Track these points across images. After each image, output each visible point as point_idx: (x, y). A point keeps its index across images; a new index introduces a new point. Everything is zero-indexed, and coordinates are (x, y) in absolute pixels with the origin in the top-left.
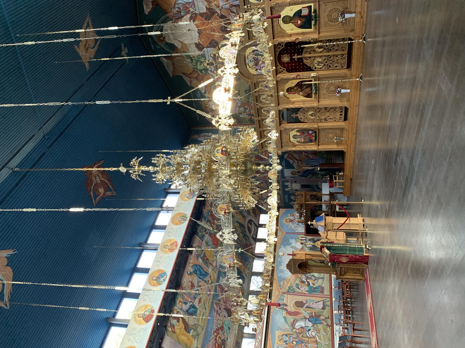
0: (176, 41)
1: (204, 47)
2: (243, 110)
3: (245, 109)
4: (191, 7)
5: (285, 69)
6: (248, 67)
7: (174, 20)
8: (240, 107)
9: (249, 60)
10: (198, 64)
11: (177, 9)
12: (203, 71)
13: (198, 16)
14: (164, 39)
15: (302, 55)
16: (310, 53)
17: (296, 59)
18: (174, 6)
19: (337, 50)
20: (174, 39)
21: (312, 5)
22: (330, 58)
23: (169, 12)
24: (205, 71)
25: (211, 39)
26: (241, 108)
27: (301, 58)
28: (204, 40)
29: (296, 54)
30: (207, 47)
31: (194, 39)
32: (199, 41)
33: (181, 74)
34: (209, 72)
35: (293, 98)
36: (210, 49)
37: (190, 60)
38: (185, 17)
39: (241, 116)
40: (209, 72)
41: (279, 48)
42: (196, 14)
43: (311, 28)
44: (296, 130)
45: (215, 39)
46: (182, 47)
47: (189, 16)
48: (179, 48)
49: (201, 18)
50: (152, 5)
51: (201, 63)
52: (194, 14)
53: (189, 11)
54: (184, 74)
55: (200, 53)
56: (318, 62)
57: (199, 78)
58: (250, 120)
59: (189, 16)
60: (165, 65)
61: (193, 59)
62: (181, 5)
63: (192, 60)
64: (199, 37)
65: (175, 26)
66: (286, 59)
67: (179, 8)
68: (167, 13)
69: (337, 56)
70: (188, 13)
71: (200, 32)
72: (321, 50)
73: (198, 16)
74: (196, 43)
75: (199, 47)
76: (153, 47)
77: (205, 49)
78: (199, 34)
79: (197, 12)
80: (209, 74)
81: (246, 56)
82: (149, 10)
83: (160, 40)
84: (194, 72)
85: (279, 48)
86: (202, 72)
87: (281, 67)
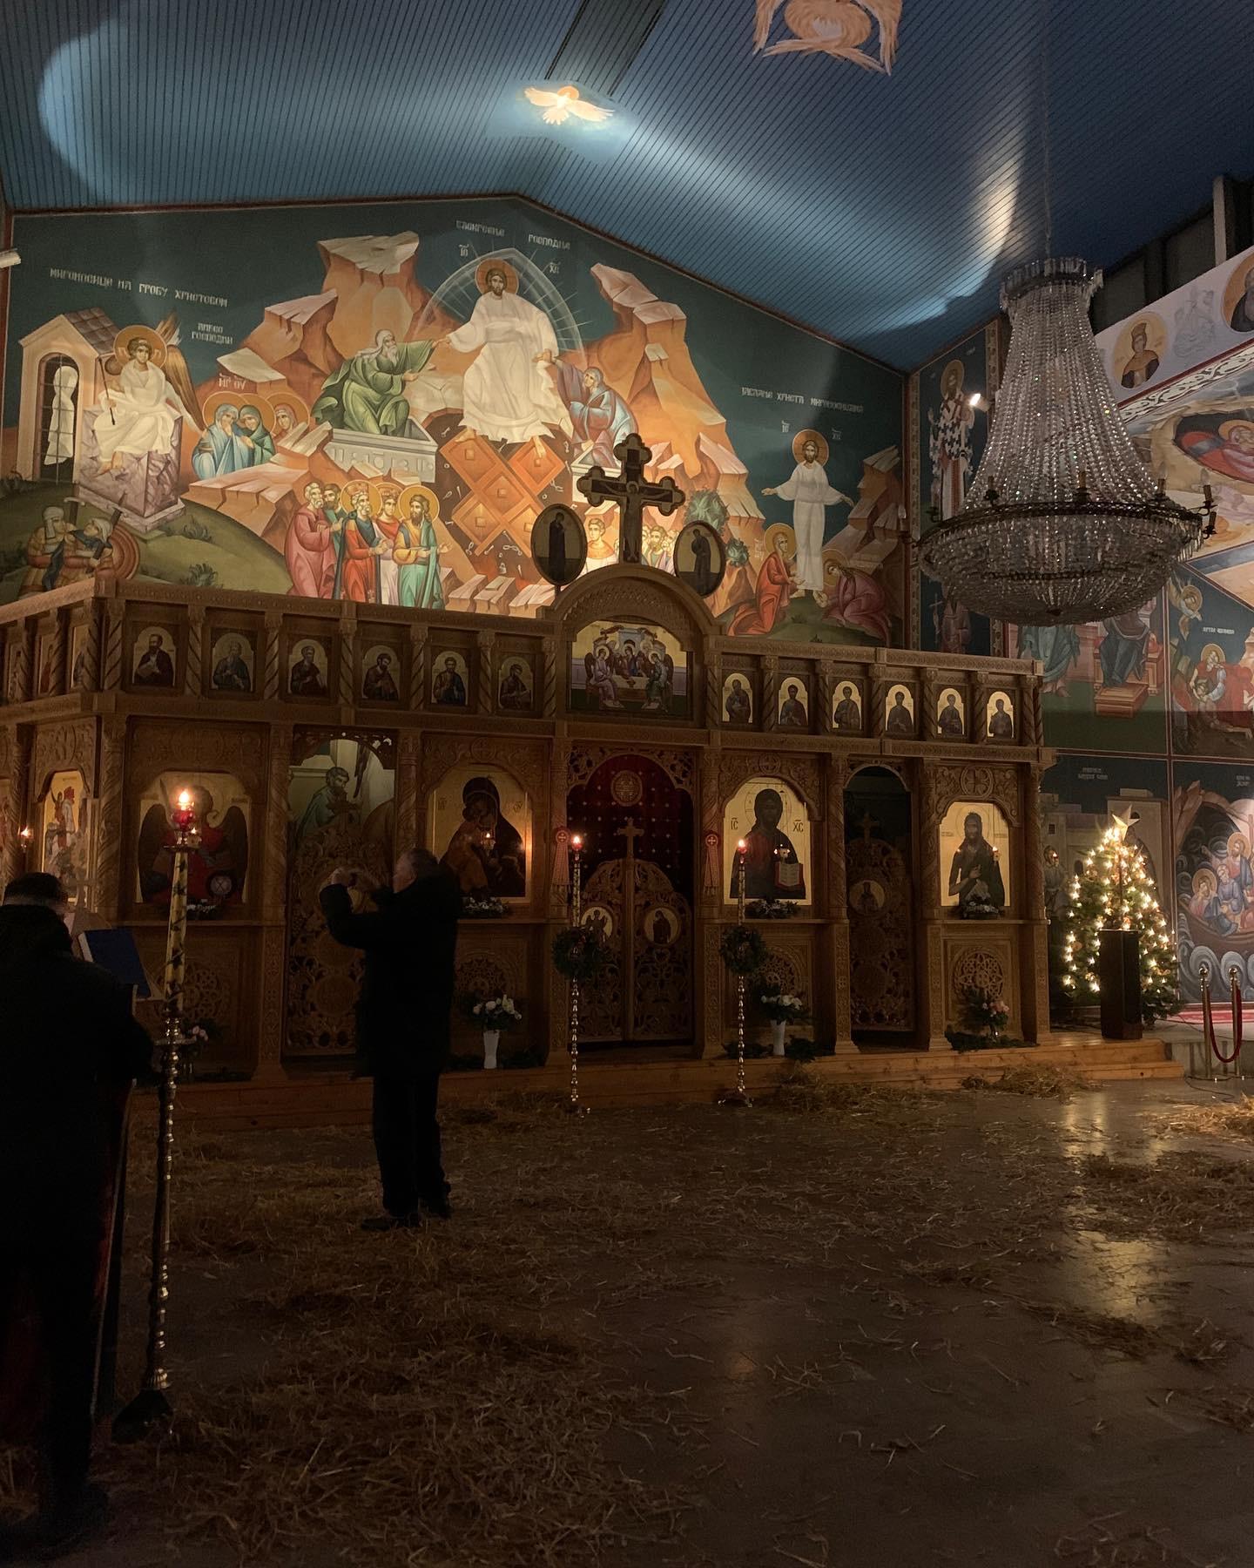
0: (480, 339)
1: (441, 442)
2: (91, 532)
3: (99, 547)
4: (595, 450)
5: (585, 782)
6: (608, 625)
7: (559, 362)
8: (115, 519)
9: (636, 638)
10: (371, 393)
11: (595, 392)
12: (333, 401)
13: (561, 466)
14: (490, 288)
15: (637, 855)
16: (637, 889)
17: (620, 831)
18: (609, 389)
19: (640, 998)
20: (488, 333)
21: (807, 901)
22: (612, 970)
23: (588, 357)
24: (330, 409)
25: (468, 481)
26: (105, 527)
27: (623, 854)
28: (470, 453)
29: (641, 832)
30: (439, 457)
31: (480, 415)
32: (468, 433)
33: (332, 294)
34: (327, 426)
35: (441, 806)
36: (433, 467)
37: (394, 361)
38: (564, 412)
39: (54, 513)
40: (327, 426)
41: (673, 768)
42: (571, 460)
43: (523, 895)
44: (246, 809)
45: (471, 502)
46: (452, 351)
47: (568, 428)
48: (451, 335)
49: (556, 472)
50: (620, 306)
51: (376, 409)
52: (572, 451)
53: (585, 439)
54: (331, 306)
55: (420, 419)
56: (603, 922)
57: (302, 367)
58: (23, 553)
59: (568, 428)
60: (382, 242)
61: (397, 378)
62: (609, 414)
63: (392, 370)
64: (485, 437)
65: (536, 360)
66: (626, 790)
67: (597, 403)
68: (588, 346)
69: (616, 998)
70: (578, 428)
71: (506, 450)
72: (650, 934)
73: (561, 466)
74: (461, 417)
75: (446, 424)
76: (539, 240)
77: (431, 445)
78: (496, 444)
79: (576, 463)
80: (318, 422)
81: (652, 629)
82: (606, 284)
83: (490, 273)
84: (333, 359)
85: (673, 768)
86: (329, 392)
87: (596, 766)
